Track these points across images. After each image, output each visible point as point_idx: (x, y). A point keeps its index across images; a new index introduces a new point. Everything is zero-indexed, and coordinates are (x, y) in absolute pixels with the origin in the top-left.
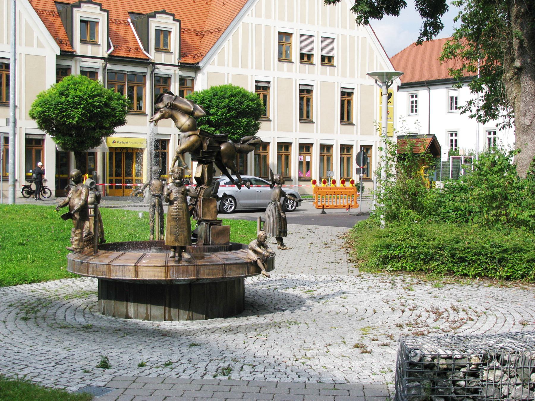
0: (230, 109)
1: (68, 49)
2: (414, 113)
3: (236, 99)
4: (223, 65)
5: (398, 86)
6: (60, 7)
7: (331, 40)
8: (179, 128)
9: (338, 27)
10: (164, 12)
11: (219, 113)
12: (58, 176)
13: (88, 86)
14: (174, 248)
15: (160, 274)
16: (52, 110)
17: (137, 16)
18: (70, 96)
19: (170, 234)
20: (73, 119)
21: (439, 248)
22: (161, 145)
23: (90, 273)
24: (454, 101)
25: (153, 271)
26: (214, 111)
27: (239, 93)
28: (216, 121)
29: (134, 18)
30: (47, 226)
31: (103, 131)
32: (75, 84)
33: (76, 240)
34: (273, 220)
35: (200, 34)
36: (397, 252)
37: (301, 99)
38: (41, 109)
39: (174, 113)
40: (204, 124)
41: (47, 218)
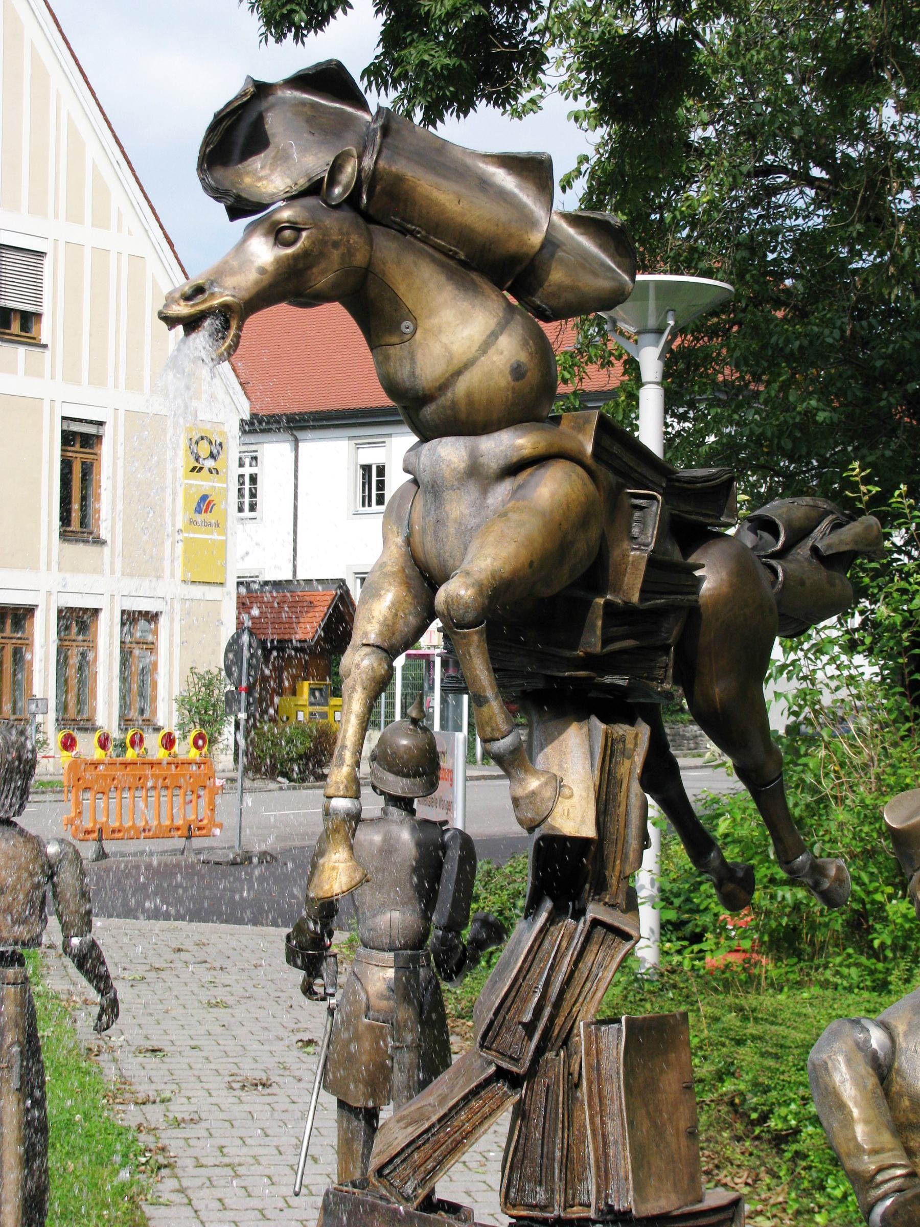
2: (247, 513)
4: (41, 375)
9: (56, 216)
24: (374, 479)
37: (66, 465)
39: (389, 251)
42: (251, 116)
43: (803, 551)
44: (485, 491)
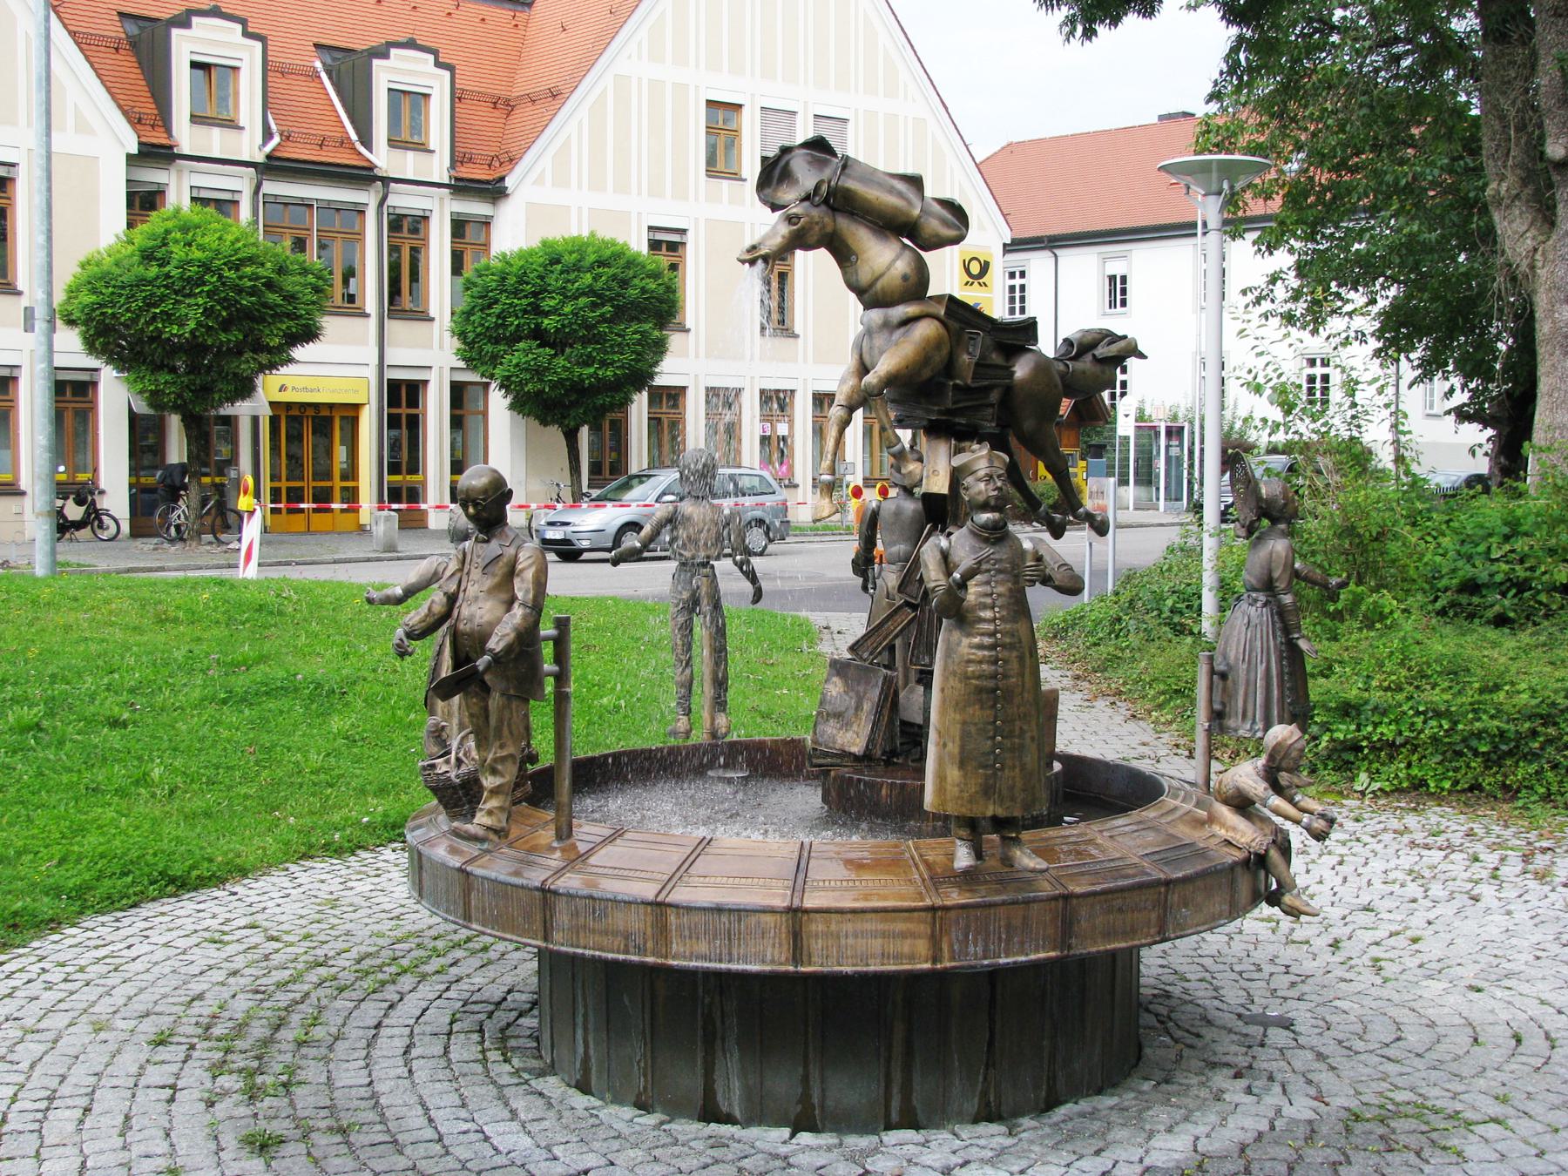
0: (599, 298)
1: (158, 138)
3: (611, 271)
5: (1005, 245)
6: (133, 29)
7: (839, 125)
8: (860, 291)
10: (411, 44)
11: (567, 309)
12: (134, 480)
13: (217, 236)
14: (972, 827)
15: (906, 947)
16: (122, 300)
17: (339, 55)
18: (174, 263)
19: (962, 765)
20: (181, 325)
21: (1541, 717)
22: (403, 397)
23: (557, 936)
24: (1119, 286)
25: (874, 934)
26: (552, 303)
27: (618, 255)
28: (557, 330)
29: (329, 61)
30: (184, 650)
31: (264, 358)
32: (185, 229)
33: (495, 792)
34: (1268, 669)
35: (505, 106)
36: (1387, 731)
38: (93, 298)
39: (844, 223)
40: (527, 337)
41: (176, 620)
42: (782, 163)
43: (1088, 357)
44: (891, 333)
